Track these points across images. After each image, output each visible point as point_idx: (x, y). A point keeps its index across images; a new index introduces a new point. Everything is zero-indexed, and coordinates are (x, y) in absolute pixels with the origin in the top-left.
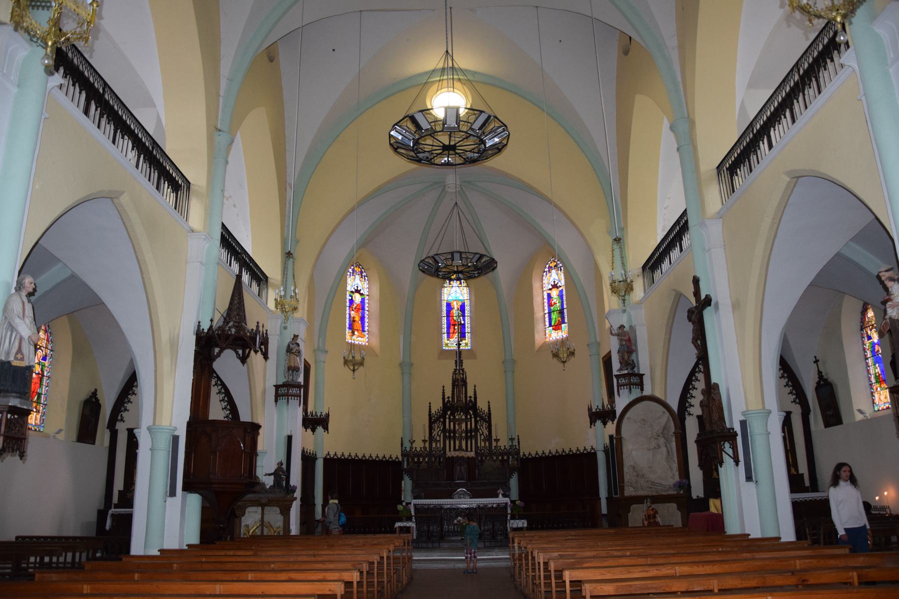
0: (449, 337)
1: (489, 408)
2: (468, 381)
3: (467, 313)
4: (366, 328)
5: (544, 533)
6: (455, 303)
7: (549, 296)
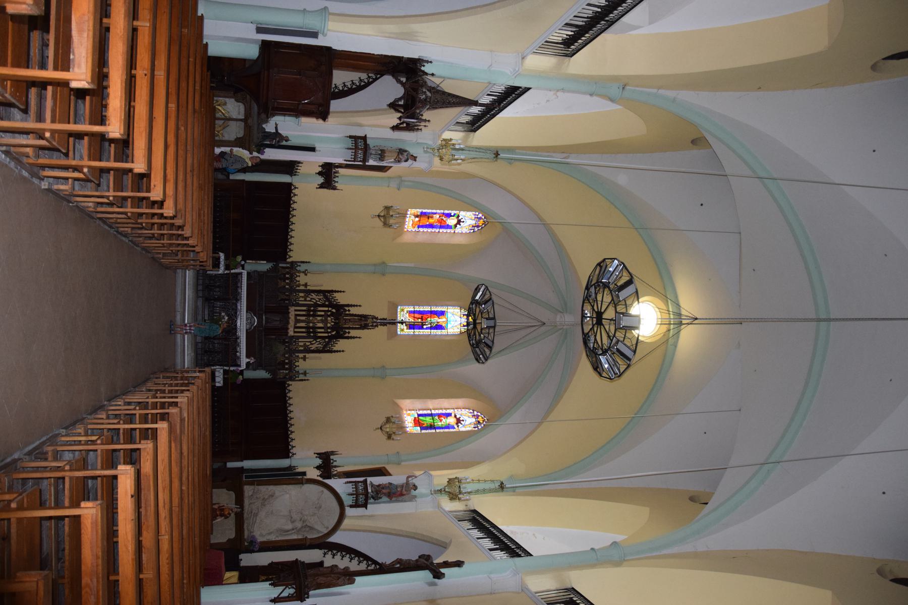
0: (410, 312)
1: (337, 351)
3: (434, 332)
4: (421, 230)
6: (444, 320)
7: (449, 415)
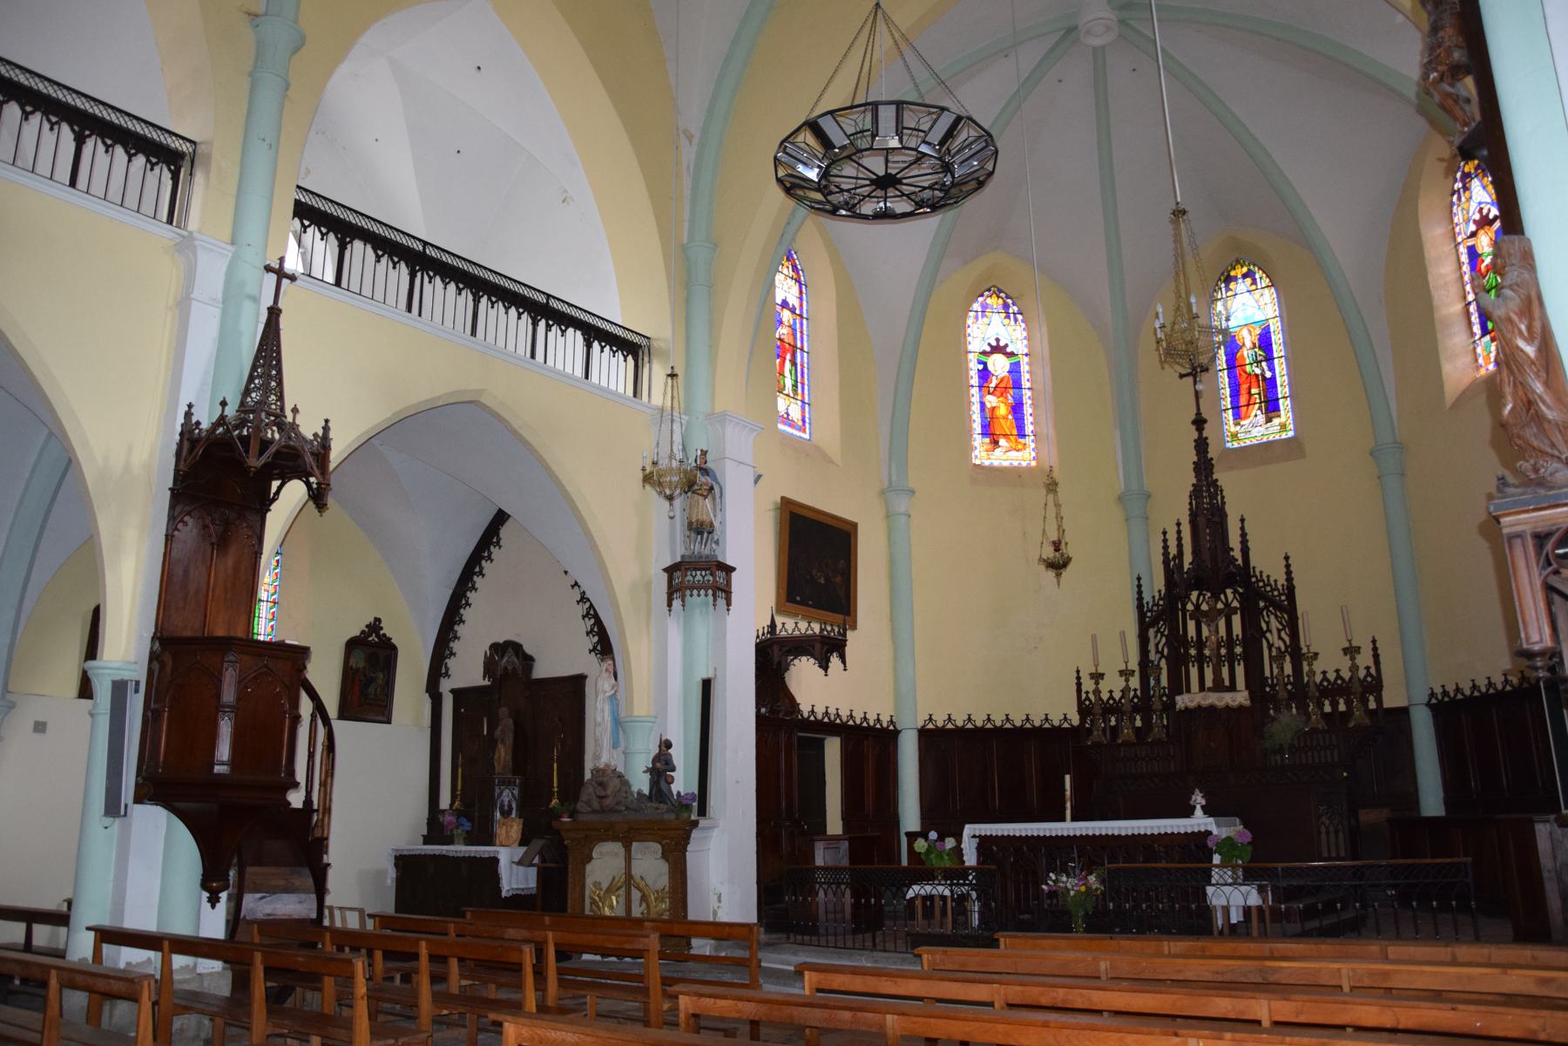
0: (1238, 416)
1: (1289, 573)
2: (1227, 508)
3: (1278, 350)
4: (1029, 429)
5: (1435, 936)
6: (1245, 332)
7: (1473, 253)
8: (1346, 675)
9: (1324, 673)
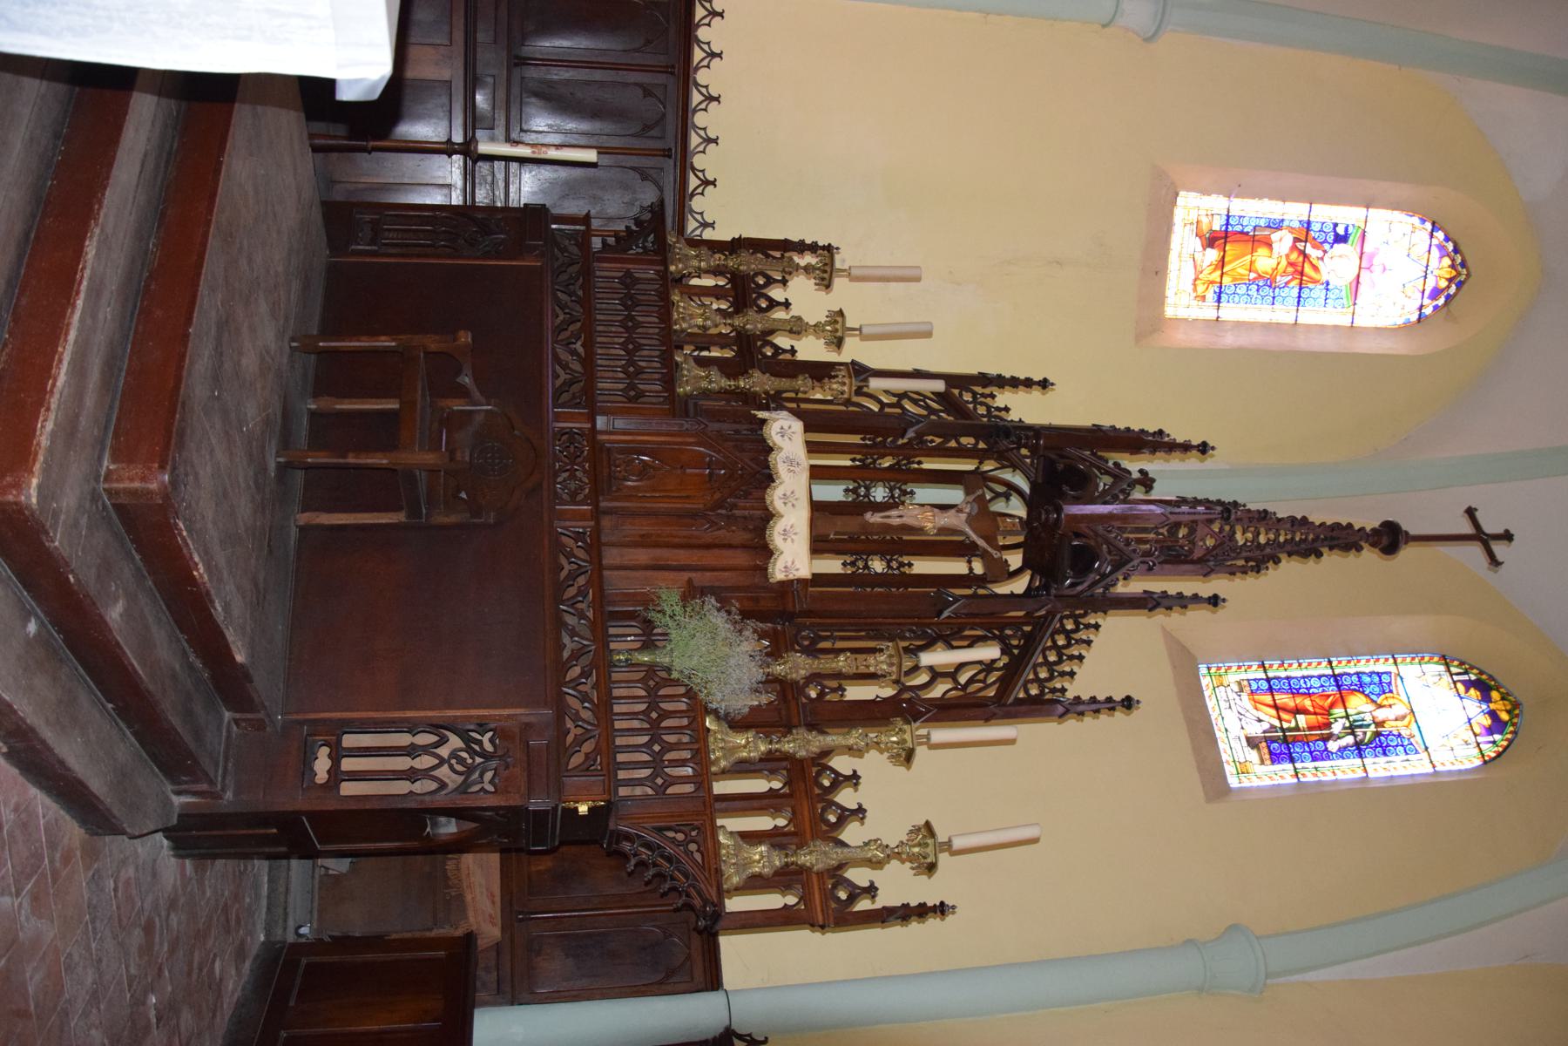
8: (852, 834)
9: (854, 779)
